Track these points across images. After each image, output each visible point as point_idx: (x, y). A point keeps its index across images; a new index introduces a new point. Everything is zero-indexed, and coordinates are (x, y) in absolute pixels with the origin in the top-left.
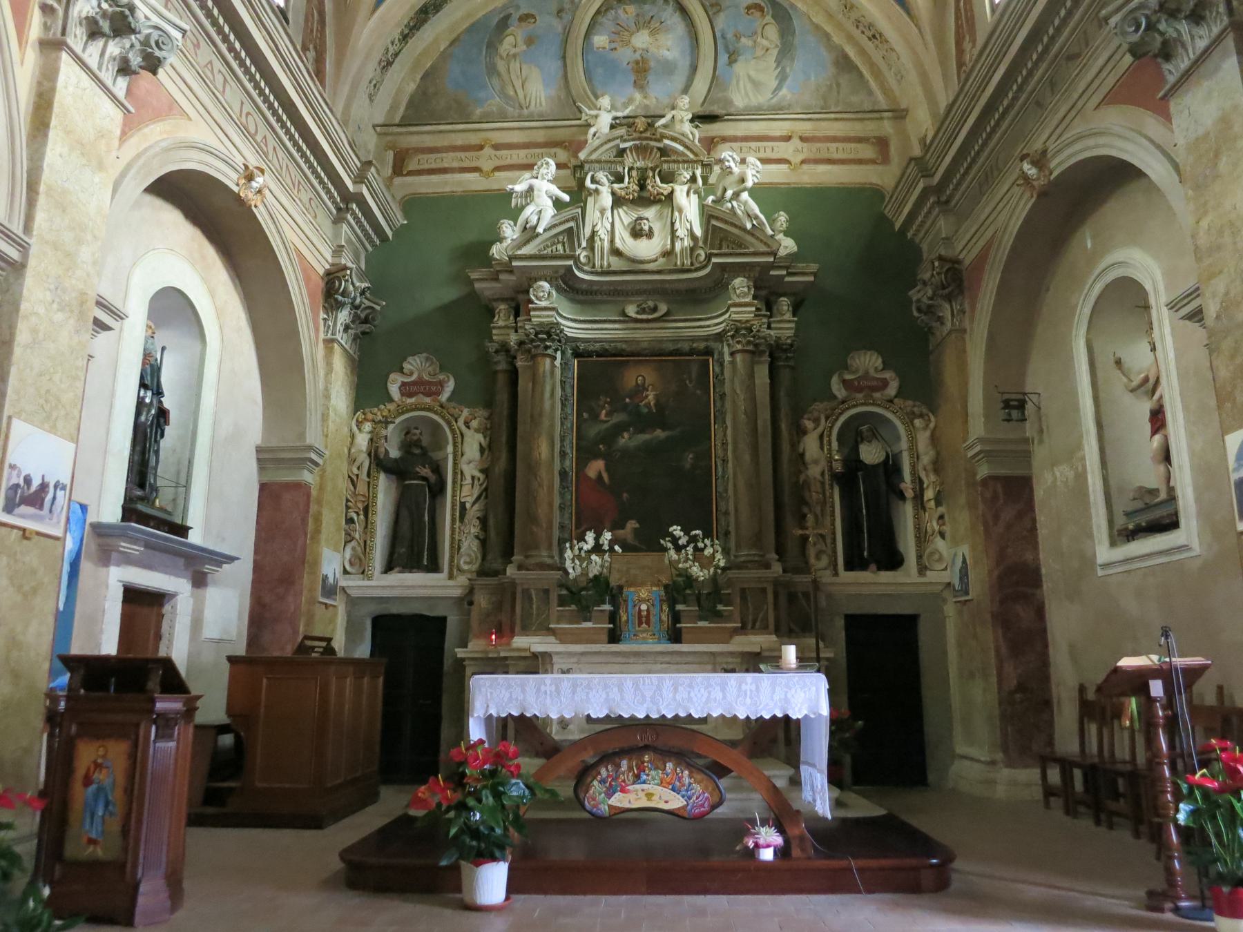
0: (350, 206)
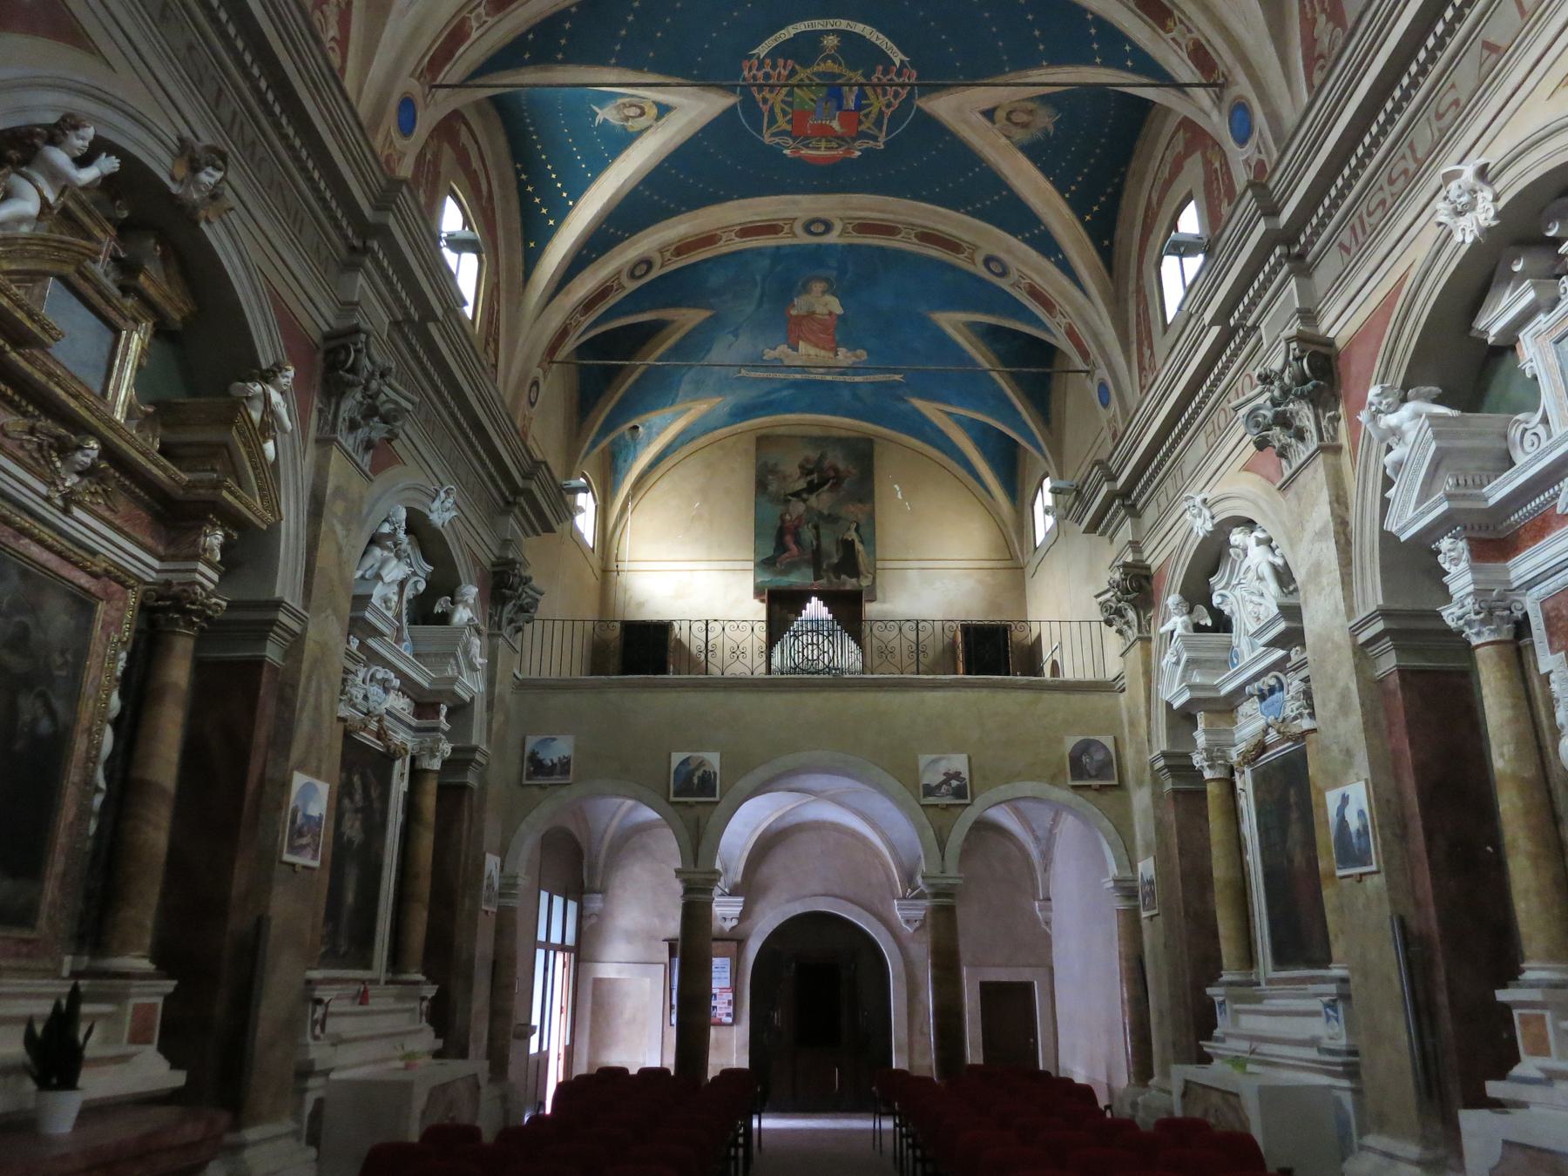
0: (517, 500)
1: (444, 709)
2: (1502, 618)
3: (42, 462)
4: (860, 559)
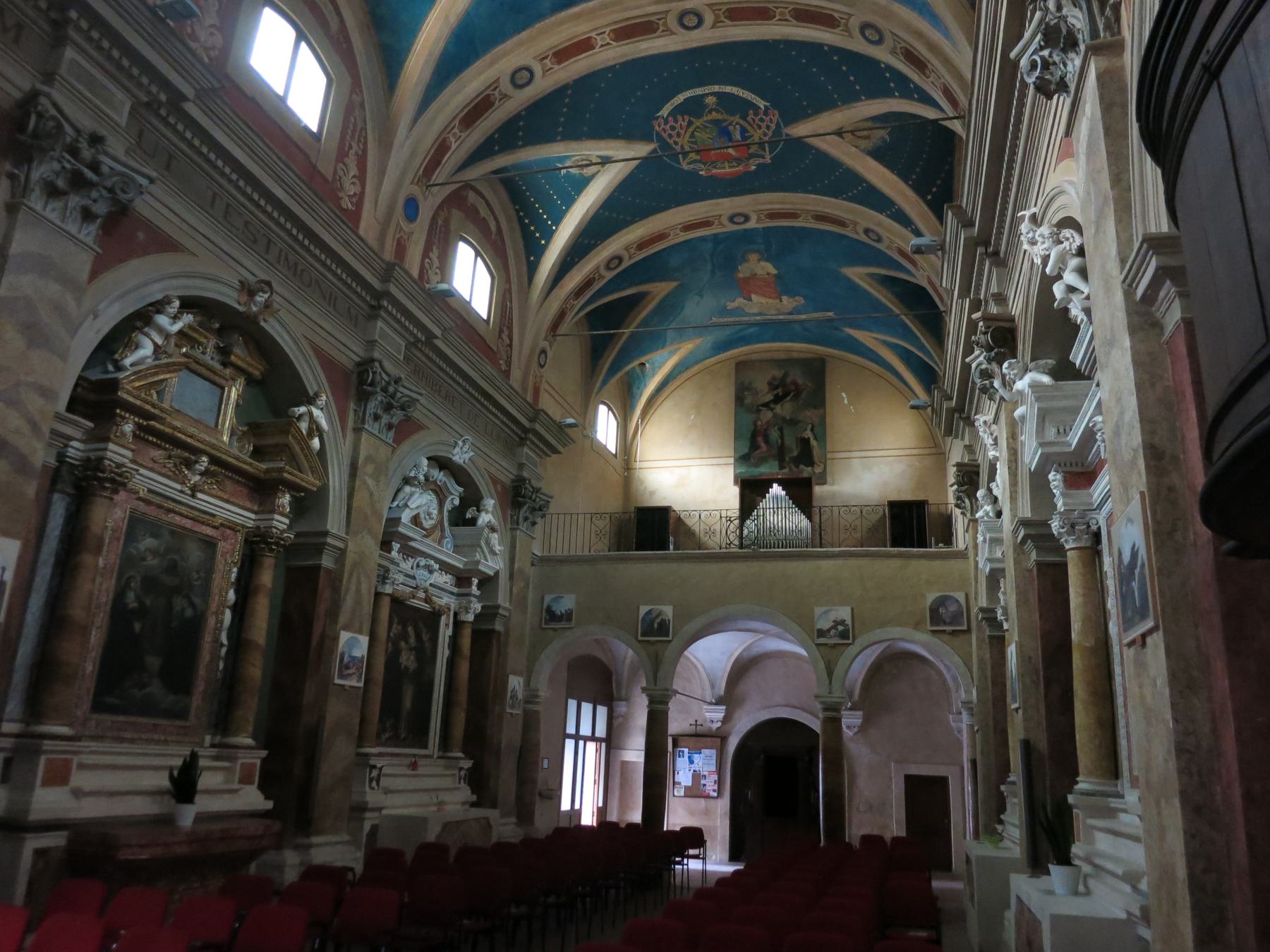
1: (475, 581)
3: (177, 472)
4: (815, 453)
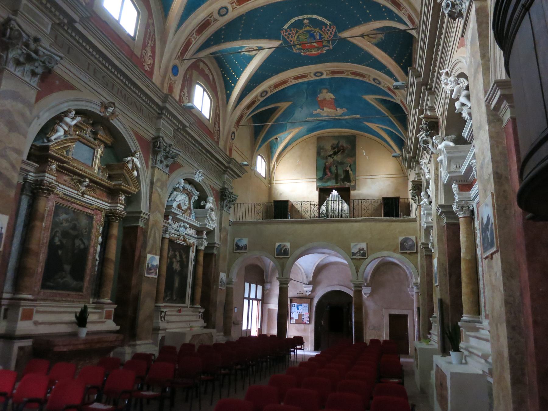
1: (205, 232)
2: (466, 210)
